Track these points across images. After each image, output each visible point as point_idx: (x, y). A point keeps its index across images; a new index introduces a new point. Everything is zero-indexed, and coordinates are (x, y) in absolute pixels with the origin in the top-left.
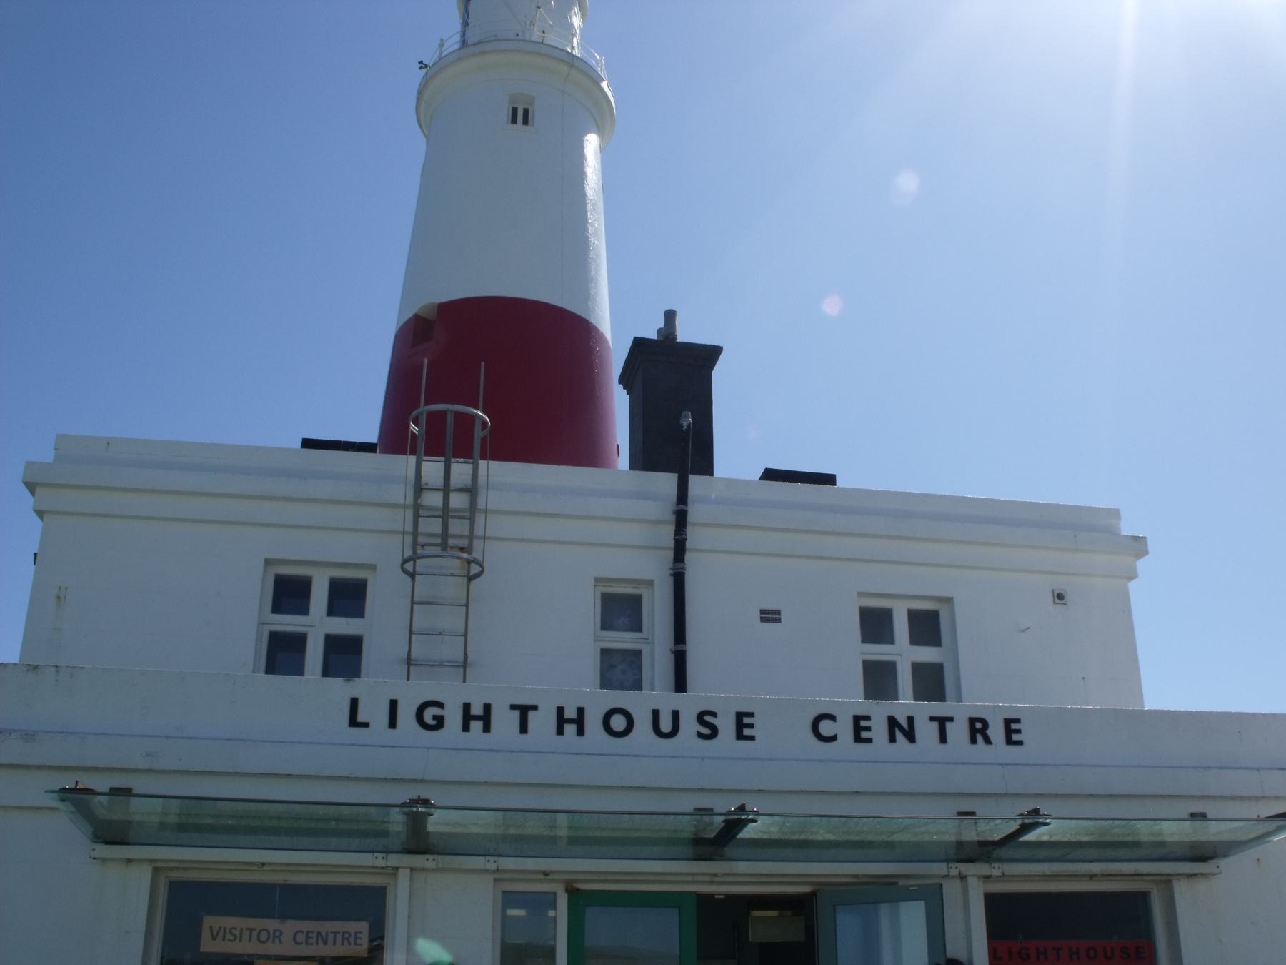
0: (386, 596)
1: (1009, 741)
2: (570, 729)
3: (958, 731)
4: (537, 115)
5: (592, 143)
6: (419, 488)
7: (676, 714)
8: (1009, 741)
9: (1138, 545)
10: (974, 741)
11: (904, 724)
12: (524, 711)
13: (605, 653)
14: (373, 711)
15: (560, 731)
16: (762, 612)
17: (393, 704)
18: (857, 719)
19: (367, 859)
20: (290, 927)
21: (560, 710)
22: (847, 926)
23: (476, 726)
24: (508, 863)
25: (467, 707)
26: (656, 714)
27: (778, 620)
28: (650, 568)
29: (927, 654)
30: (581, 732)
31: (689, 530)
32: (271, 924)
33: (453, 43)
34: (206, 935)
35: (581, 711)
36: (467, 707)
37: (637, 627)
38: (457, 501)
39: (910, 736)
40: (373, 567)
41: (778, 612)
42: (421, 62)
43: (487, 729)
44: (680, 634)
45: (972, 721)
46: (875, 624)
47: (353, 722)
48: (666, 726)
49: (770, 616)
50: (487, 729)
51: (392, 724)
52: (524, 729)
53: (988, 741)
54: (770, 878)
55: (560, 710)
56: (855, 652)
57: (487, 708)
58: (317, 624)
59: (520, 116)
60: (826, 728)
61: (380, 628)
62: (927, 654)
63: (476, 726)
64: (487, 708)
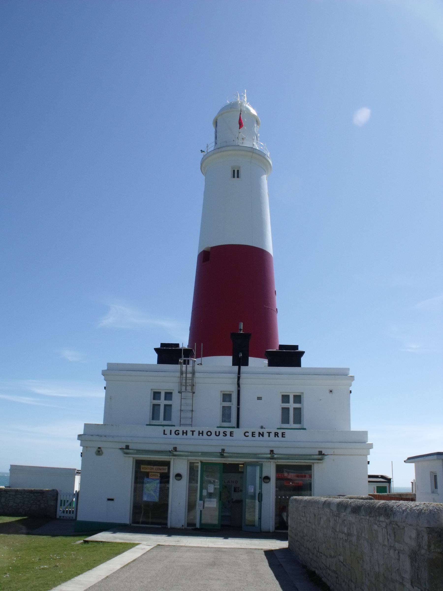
0: (176, 396)
1: (282, 437)
2: (201, 435)
3: (272, 435)
4: (241, 173)
5: (265, 178)
6: (182, 373)
7: (219, 432)
8: (282, 437)
9: (352, 378)
10: (275, 437)
11: (262, 433)
12: (193, 432)
13: (223, 407)
14: (168, 432)
15: (199, 435)
16: (258, 398)
17: (171, 431)
18: (253, 432)
19: (166, 457)
20: (155, 467)
21: (199, 431)
22: (249, 469)
23: (185, 434)
24: (189, 458)
25: (183, 431)
26: (216, 432)
27: (261, 399)
28: (232, 388)
29: (297, 406)
30: (202, 435)
31: (241, 380)
32: (152, 467)
33: (212, 147)
34: (142, 468)
35: (203, 432)
36: (183, 431)
37: (230, 401)
39: (263, 436)
40: (173, 390)
41: (261, 398)
42: (201, 150)
43: (186, 435)
45: (275, 433)
46: (285, 399)
47: (164, 434)
48: (217, 434)
49: (259, 398)
50: (186, 435)
51: (171, 434)
52: (193, 435)
53: (278, 437)
54: (234, 461)
55: (199, 431)
56: (279, 405)
57: (187, 431)
58: (162, 402)
59: (236, 174)
60: (247, 434)
61: (175, 402)
62: (297, 406)
63: (185, 434)
64: (187, 431)
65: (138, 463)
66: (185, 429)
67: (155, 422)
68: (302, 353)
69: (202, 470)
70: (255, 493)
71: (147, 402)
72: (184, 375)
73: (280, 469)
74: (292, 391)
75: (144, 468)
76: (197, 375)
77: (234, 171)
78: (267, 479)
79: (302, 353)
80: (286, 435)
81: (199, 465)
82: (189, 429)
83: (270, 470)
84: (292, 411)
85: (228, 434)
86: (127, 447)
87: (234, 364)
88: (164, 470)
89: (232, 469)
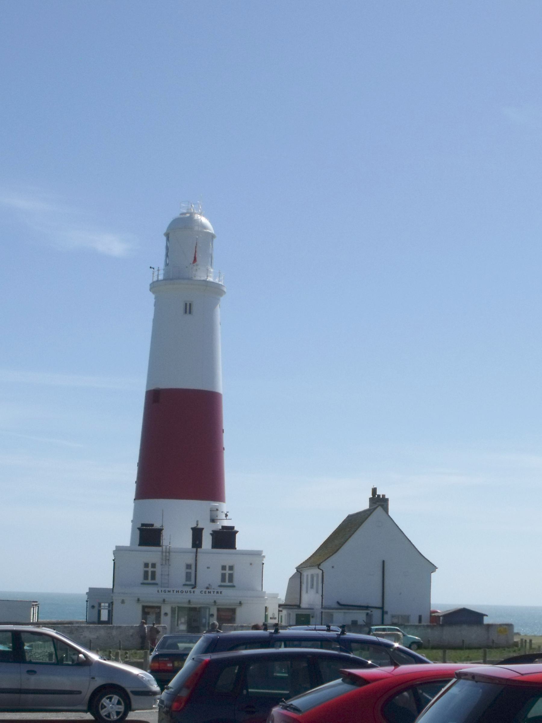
0: (158, 566)
3: (215, 593)
4: (194, 309)
14: (160, 591)
28: (191, 561)
38: (167, 554)
44: (196, 571)
46: (224, 568)
49: (208, 568)
56: (220, 572)
59: (188, 309)
61: (158, 570)
65: (144, 607)
66: (169, 589)
67: (146, 581)
68: (237, 532)
69: (177, 611)
70: (206, 622)
71: (141, 570)
72: (164, 554)
73: (218, 610)
74: (228, 564)
75: (146, 610)
76: (171, 554)
77: (186, 304)
78: (212, 615)
79: (237, 532)
80: (223, 593)
81: (430, 698)
82: (171, 589)
83: (214, 611)
84: (228, 577)
85: (192, 592)
86: (138, 600)
87: (193, 547)
88: (158, 610)
89: (194, 609)
